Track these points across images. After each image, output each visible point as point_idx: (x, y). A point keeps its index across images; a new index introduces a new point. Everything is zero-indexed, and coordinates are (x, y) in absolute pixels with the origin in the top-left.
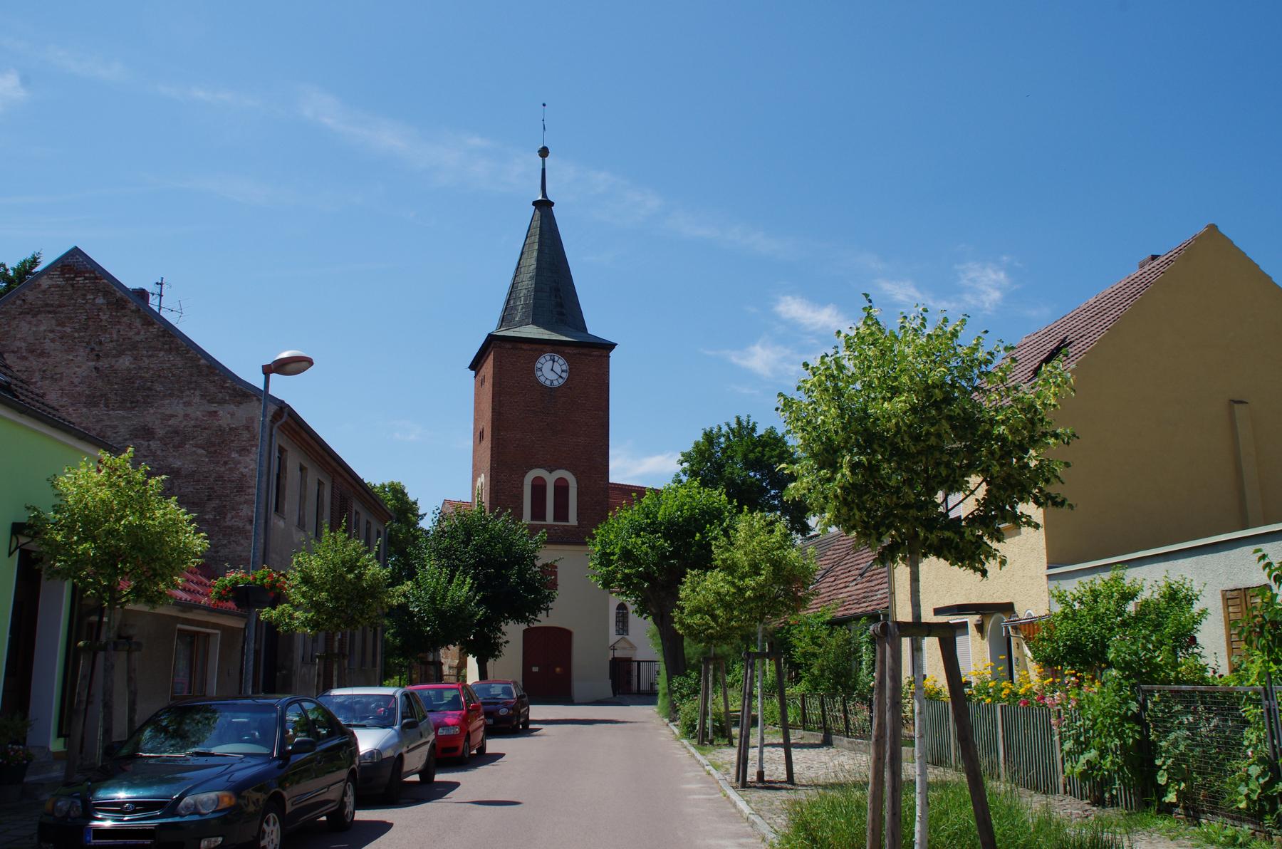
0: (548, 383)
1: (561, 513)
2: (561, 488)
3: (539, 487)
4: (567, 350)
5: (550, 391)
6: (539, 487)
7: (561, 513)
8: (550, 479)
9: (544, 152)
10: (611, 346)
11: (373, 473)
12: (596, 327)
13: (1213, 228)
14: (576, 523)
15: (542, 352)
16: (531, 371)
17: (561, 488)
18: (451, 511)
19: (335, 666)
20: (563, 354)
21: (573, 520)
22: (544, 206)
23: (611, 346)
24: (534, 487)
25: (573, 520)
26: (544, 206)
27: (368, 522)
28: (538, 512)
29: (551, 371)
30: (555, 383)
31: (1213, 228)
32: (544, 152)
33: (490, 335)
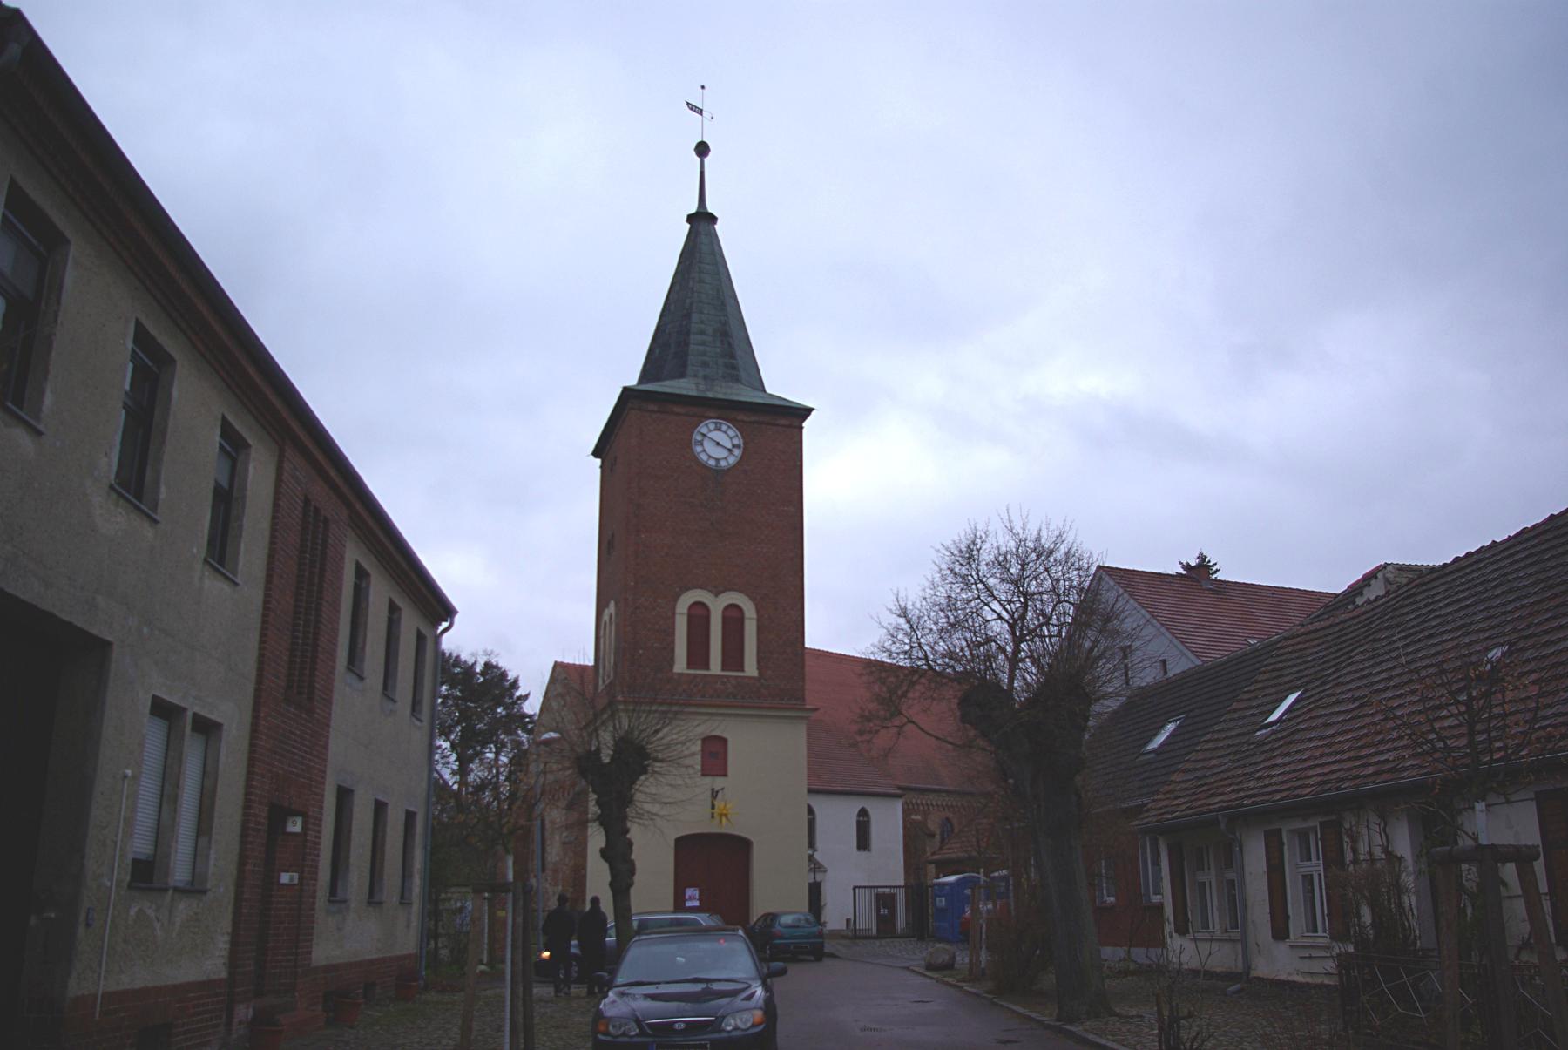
0: (712, 463)
1: (733, 657)
2: (733, 619)
3: (699, 616)
4: (741, 417)
5: (716, 475)
6: (699, 616)
7: (733, 657)
8: (716, 606)
9: (702, 149)
10: (807, 412)
11: (606, 866)
12: (779, 382)
13: (725, 775)
14: (755, 674)
15: (703, 418)
16: (687, 445)
17: (733, 619)
18: (562, 674)
19: (1171, 727)
20: (733, 421)
21: (751, 669)
22: (702, 220)
23: (807, 412)
24: (690, 617)
25: (751, 669)
26: (702, 220)
27: (393, 608)
28: (698, 655)
29: (718, 445)
30: (723, 463)
31: (725, 775)
32: (702, 149)
33: (625, 389)
